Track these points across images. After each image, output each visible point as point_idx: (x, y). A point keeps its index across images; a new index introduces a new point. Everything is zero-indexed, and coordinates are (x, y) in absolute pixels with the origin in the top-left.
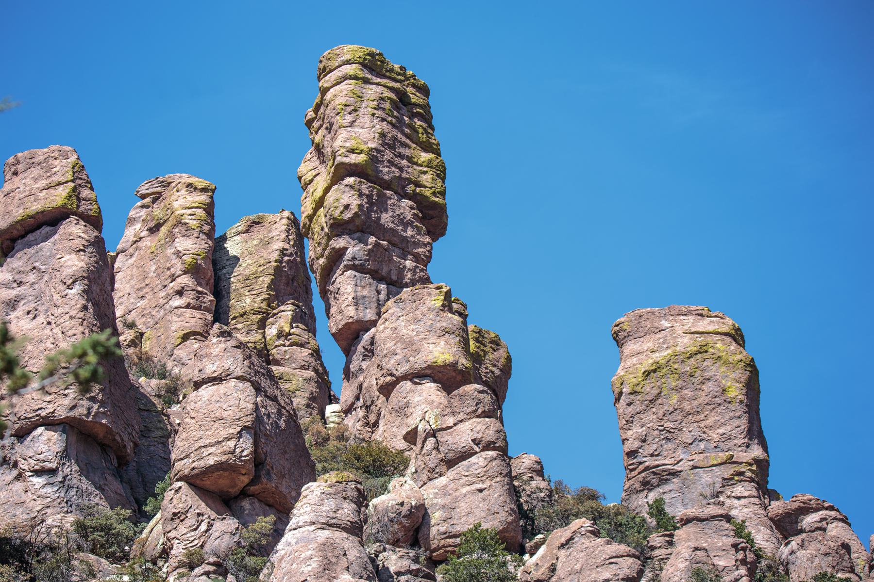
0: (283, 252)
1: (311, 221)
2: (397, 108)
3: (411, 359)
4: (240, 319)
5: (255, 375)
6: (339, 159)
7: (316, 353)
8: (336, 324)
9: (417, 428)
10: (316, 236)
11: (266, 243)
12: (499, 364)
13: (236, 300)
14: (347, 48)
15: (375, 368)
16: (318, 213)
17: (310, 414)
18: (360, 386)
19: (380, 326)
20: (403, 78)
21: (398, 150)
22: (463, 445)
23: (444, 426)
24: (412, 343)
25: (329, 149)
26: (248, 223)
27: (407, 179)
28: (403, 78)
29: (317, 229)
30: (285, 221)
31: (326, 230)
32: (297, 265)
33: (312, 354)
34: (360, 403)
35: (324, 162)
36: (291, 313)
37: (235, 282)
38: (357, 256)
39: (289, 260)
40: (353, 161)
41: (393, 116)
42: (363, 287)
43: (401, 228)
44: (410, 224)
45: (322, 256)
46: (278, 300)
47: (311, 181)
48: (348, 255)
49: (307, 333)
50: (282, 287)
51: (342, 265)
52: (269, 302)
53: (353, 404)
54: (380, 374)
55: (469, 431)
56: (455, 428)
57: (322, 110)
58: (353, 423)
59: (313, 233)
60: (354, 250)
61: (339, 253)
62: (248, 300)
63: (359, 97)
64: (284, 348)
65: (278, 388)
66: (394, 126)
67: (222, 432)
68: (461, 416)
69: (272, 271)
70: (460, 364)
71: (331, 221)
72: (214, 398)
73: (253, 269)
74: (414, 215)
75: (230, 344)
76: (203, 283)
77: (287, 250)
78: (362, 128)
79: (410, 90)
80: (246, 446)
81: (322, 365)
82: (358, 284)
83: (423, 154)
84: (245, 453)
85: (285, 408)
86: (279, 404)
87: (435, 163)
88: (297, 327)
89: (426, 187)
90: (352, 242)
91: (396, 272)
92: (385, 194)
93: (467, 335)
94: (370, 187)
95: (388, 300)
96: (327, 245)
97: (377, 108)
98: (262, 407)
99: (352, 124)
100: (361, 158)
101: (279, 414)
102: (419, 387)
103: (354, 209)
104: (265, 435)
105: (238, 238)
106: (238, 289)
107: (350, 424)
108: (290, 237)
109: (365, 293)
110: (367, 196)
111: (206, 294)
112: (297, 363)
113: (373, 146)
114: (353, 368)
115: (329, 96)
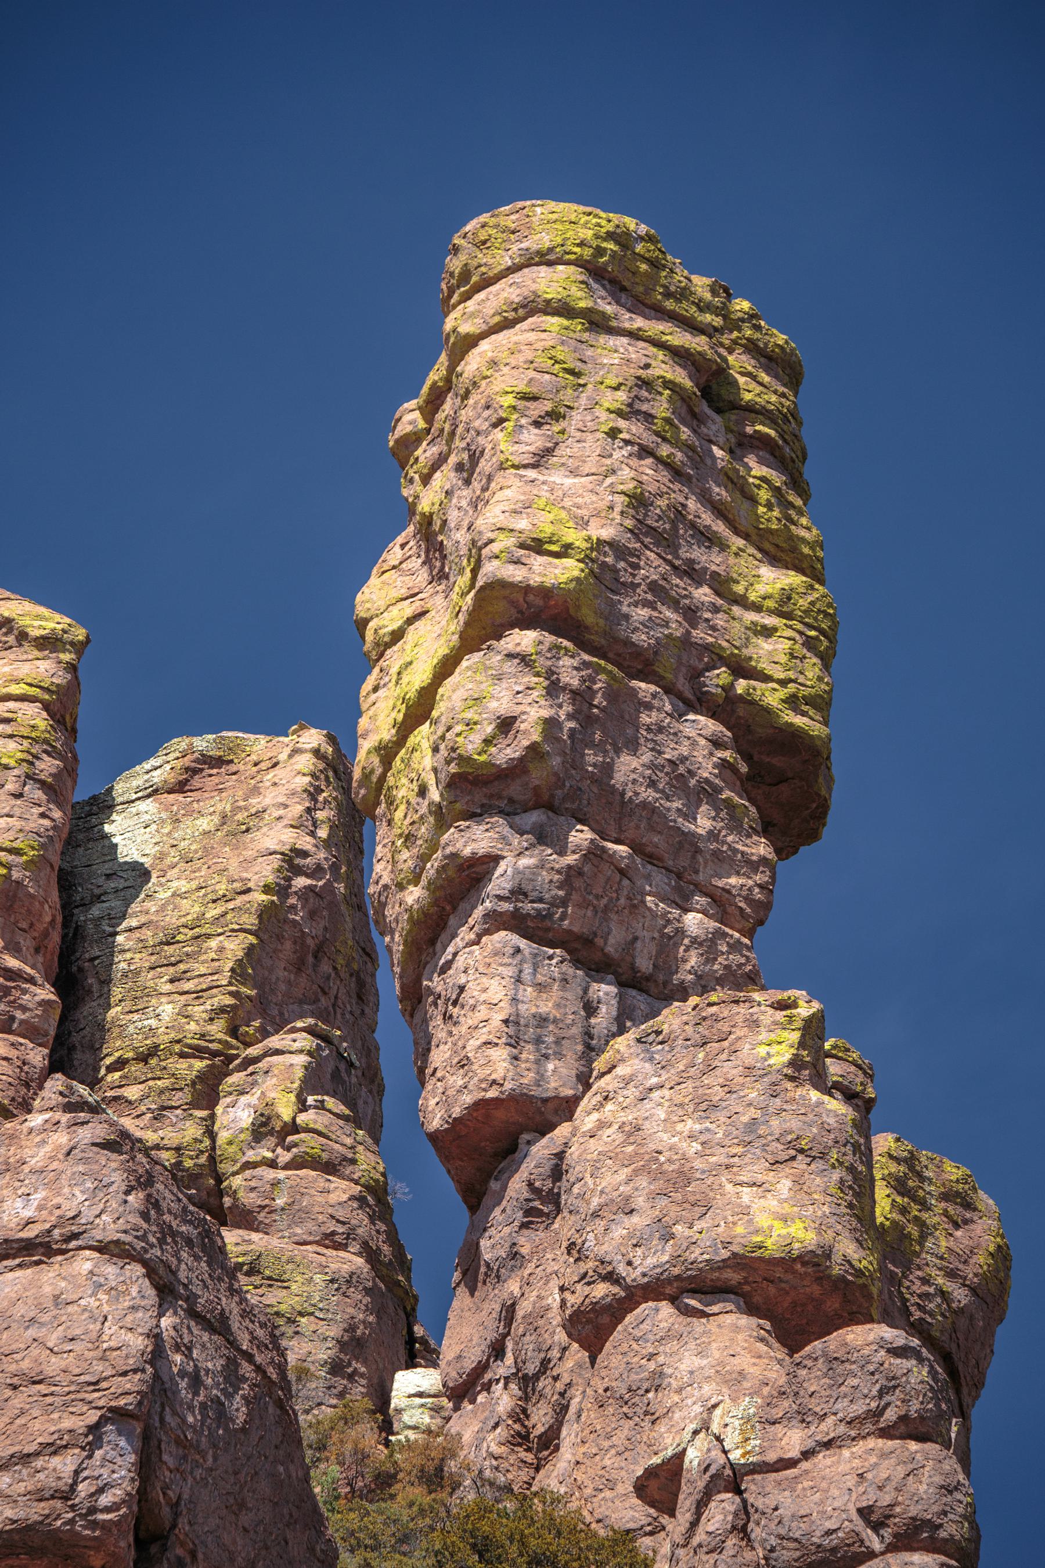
0: (292, 861)
1: (387, 762)
2: (694, 419)
3: (678, 1229)
4: (135, 1069)
5: (162, 1241)
6: (491, 569)
7: (376, 1198)
8: (446, 1102)
9: (681, 1455)
10: (399, 814)
11: (238, 828)
12: (969, 1271)
13: (127, 1005)
14: (542, 210)
15: (561, 1252)
16: (411, 741)
17: (341, 1395)
18: (509, 1312)
19: (586, 1119)
20: (718, 322)
21: (683, 553)
22: (830, 1525)
23: (771, 1457)
24: (684, 1177)
25: (461, 537)
26: (187, 761)
27: (707, 648)
28: (718, 322)
29: (404, 790)
30: (306, 762)
31: (435, 795)
32: (333, 905)
33: (360, 1199)
34: (504, 1368)
35: (441, 576)
36: (302, 1059)
37: (129, 949)
38: (527, 887)
39: (310, 888)
40: (535, 580)
41: (676, 443)
42: (541, 987)
43: (677, 804)
44: (706, 793)
45: (416, 880)
46: (264, 1013)
47: (397, 636)
48: (501, 881)
49: (349, 1128)
50: (282, 974)
51: (479, 912)
52: (235, 1019)
53: (482, 1368)
54: (571, 1274)
55: (851, 1481)
56: (805, 1465)
57: (448, 406)
58: (478, 1437)
59: (390, 802)
60: (515, 859)
61: (473, 873)
62: (168, 1010)
63: (571, 372)
64: (270, 1174)
65: (233, 1291)
66: (677, 473)
67: (37, 1425)
68: (828, 1428)
69: (250, 921)
70: (837, 1258)
71: (453, 768)
72: (21, 1310)
73: (191, 908)
74: (724, 764)
75: (85, 1135)
76: (26, 943)
77: (305, 854)
78: (574, 473)
79: (738, 361)
80: (112, 1475)
81: (392, 1237)
82: (526, 975)
83: (767, 572)
84: (105, 1500)
85: (249, 1357)
86: (232, 1343)
87: (803, 603)
88: (321, 1106)
89: (767, 678)
90: (516, 840)
91: (653, 949)
92: (634, 692)
93: (870, 1166)
94: (586, 665)
95: (622, 1031)
96: (433, 846)
97: (628, 412)
98: (177, 1348)
99: (541, 459)
100: (562, 572)
101: (231, 1376)
102: (699, 1325)
103: (530, 731)
104: (178, 1442)
105: (148, 806)
106: (137, 973)
107: (467, 1437)
108: (320, 815)
109: (546, 1007)
110: (575, 693)
111: (31, 980)
112: (311, 1226)
113: (607, 533)
114: (490, 1248)
115: (472, 364)
